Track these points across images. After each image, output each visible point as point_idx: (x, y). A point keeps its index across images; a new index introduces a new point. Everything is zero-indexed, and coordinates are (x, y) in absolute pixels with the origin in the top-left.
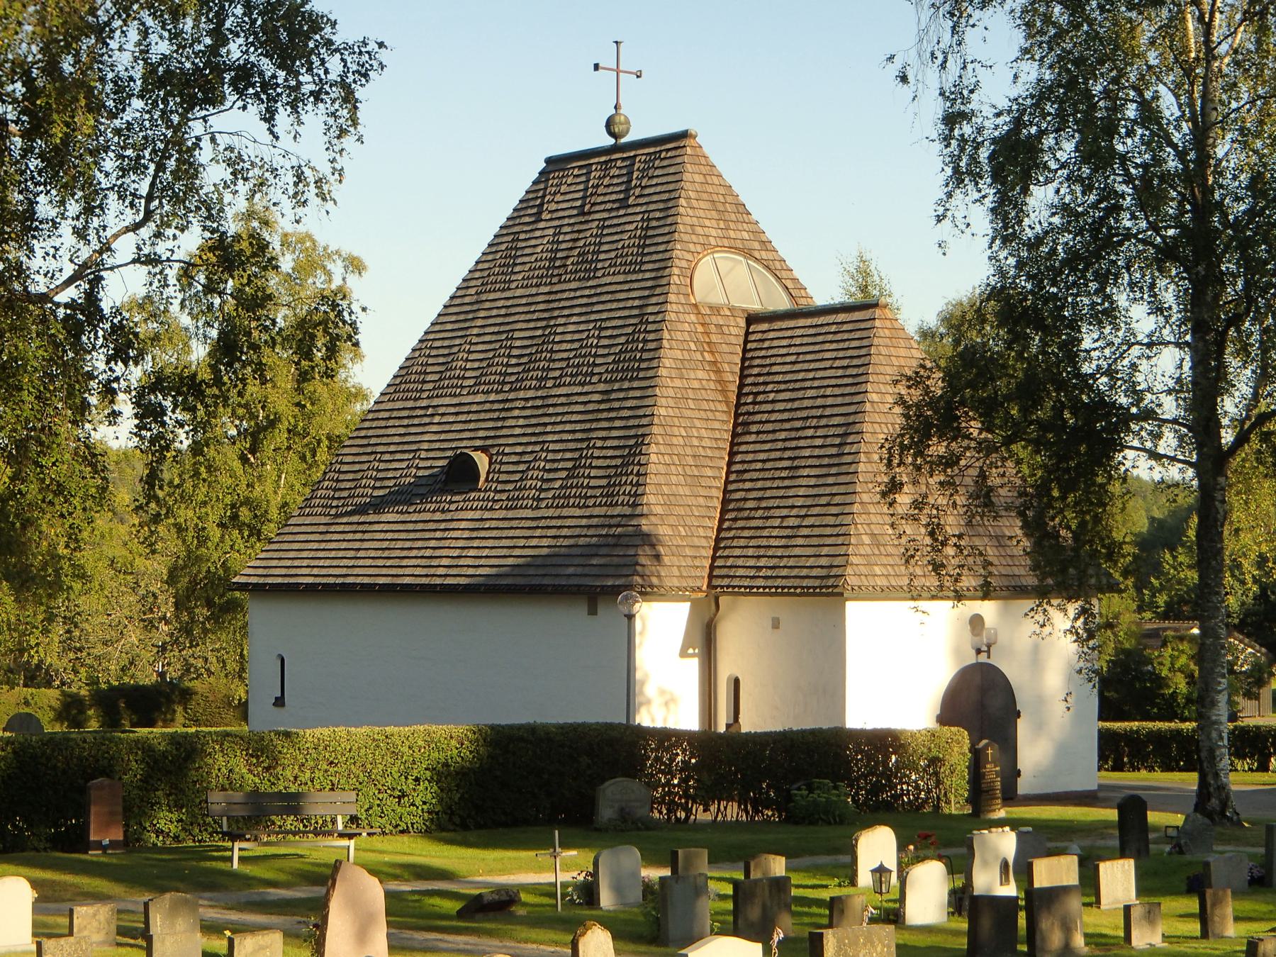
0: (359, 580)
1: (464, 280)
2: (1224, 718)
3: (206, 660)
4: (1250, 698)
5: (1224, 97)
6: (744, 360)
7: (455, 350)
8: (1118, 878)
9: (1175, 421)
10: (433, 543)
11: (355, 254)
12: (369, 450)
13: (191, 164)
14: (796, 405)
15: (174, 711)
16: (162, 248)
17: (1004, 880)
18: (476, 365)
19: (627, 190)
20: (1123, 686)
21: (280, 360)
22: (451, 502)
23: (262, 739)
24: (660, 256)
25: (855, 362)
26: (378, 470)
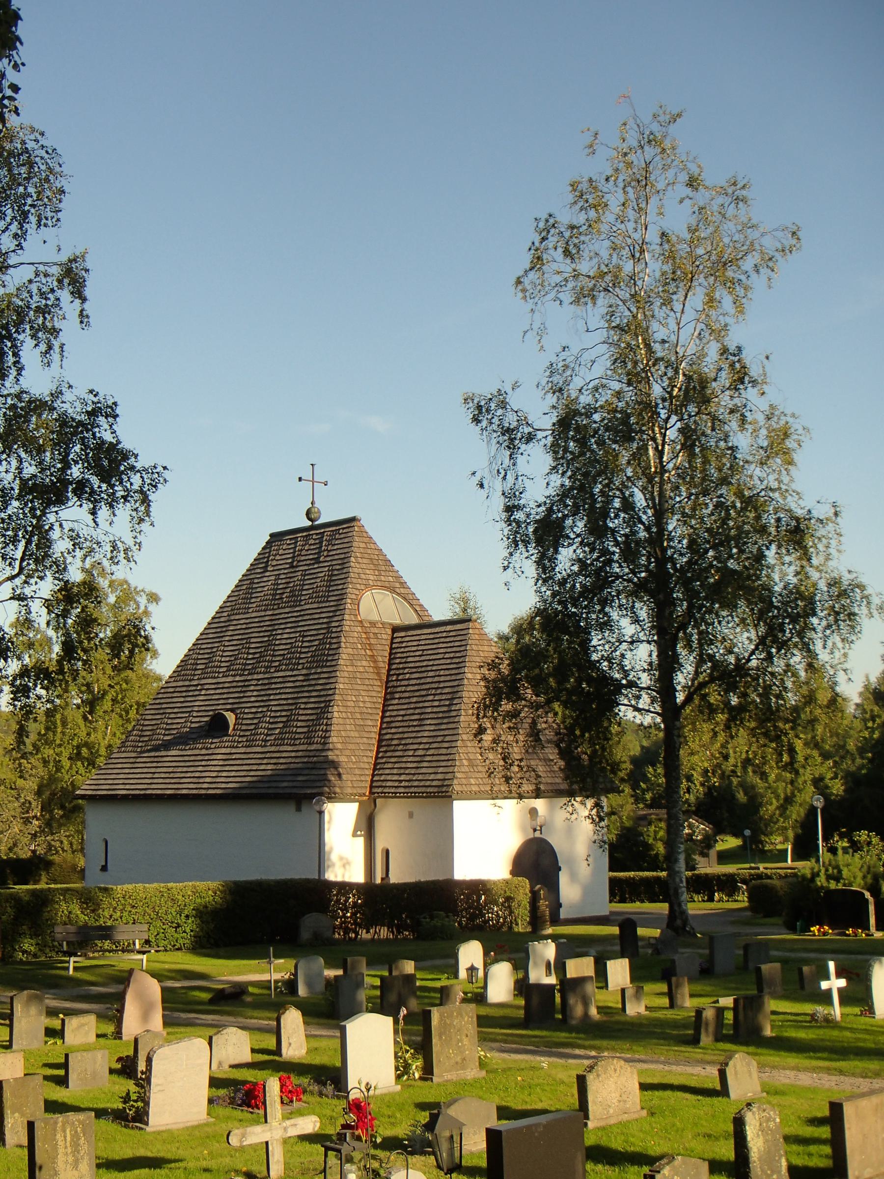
0: (154, 792)
1: (221, 608)
2: (683, 870)
3: (62, 842)
4: (703, 857)
5: (672, 494)
6: (390, 654)
7: (214, 650)
8: (619, 971)
9: (648, 688)
10: (200, 769)
11: (154, 591)
12: (161, 711)
13: (48, 540)
14: (422, 681)
15: (41, 875)
16: (28, 591)
17: (549, 973)
18: (228, 659)
19: (319, 553)
22: (212, 743)
23: (90, 892)
24: (339, 592)
25: (458, 655)
26: (167, 724)
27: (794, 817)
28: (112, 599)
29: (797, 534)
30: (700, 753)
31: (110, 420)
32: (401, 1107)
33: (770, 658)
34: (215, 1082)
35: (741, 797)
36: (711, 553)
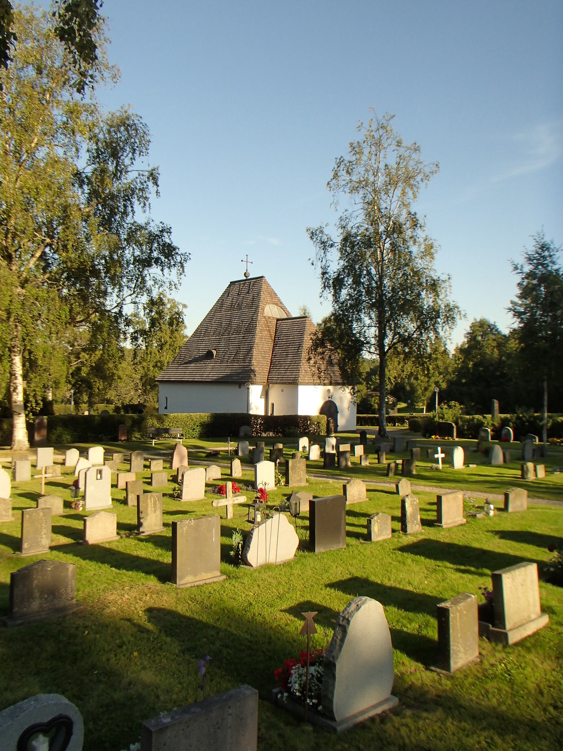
2: (385, 413)
8: (359, 450)
16: (137, 300)
17: (333, 449)
20: (363, 406)
21: (165, 327)
27: (427, 396)
28: (169, 306)
29: (434, 286)
30: (393, 371)
31: (169, 234)
32: (276, 495)
33: (421, 334)
34: (207, 485)
35: (408, 388)
36: (400, 293)
